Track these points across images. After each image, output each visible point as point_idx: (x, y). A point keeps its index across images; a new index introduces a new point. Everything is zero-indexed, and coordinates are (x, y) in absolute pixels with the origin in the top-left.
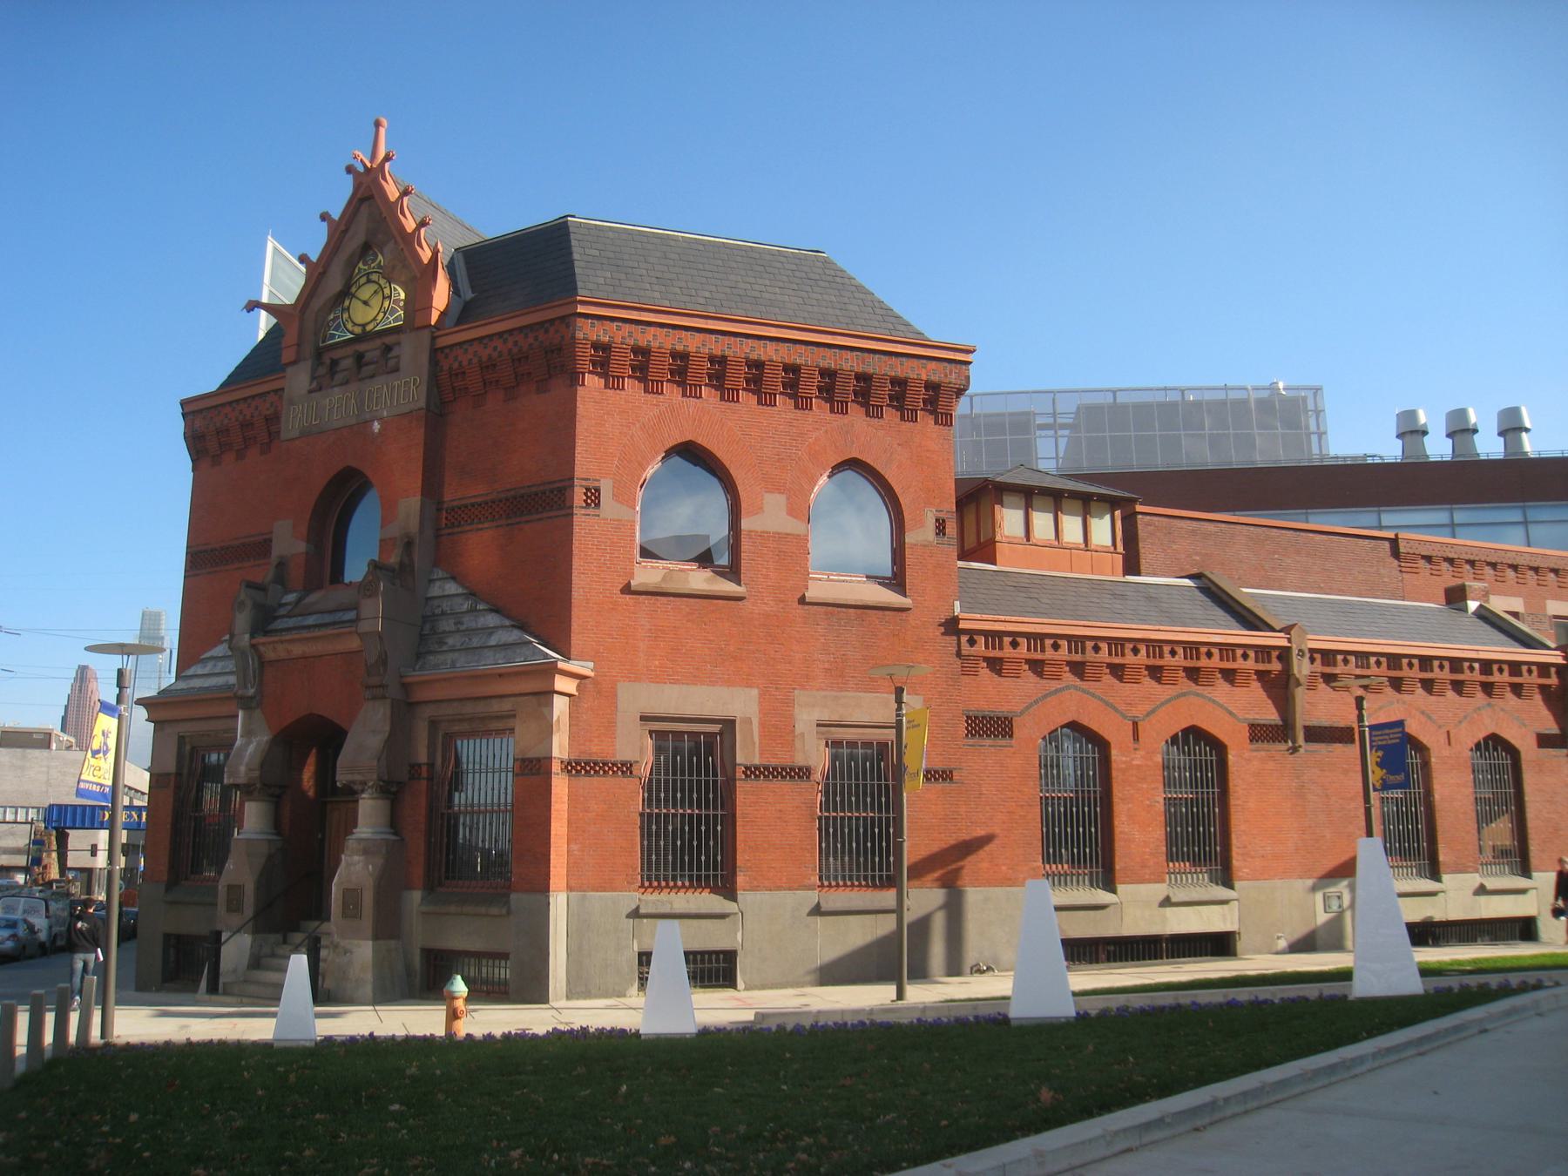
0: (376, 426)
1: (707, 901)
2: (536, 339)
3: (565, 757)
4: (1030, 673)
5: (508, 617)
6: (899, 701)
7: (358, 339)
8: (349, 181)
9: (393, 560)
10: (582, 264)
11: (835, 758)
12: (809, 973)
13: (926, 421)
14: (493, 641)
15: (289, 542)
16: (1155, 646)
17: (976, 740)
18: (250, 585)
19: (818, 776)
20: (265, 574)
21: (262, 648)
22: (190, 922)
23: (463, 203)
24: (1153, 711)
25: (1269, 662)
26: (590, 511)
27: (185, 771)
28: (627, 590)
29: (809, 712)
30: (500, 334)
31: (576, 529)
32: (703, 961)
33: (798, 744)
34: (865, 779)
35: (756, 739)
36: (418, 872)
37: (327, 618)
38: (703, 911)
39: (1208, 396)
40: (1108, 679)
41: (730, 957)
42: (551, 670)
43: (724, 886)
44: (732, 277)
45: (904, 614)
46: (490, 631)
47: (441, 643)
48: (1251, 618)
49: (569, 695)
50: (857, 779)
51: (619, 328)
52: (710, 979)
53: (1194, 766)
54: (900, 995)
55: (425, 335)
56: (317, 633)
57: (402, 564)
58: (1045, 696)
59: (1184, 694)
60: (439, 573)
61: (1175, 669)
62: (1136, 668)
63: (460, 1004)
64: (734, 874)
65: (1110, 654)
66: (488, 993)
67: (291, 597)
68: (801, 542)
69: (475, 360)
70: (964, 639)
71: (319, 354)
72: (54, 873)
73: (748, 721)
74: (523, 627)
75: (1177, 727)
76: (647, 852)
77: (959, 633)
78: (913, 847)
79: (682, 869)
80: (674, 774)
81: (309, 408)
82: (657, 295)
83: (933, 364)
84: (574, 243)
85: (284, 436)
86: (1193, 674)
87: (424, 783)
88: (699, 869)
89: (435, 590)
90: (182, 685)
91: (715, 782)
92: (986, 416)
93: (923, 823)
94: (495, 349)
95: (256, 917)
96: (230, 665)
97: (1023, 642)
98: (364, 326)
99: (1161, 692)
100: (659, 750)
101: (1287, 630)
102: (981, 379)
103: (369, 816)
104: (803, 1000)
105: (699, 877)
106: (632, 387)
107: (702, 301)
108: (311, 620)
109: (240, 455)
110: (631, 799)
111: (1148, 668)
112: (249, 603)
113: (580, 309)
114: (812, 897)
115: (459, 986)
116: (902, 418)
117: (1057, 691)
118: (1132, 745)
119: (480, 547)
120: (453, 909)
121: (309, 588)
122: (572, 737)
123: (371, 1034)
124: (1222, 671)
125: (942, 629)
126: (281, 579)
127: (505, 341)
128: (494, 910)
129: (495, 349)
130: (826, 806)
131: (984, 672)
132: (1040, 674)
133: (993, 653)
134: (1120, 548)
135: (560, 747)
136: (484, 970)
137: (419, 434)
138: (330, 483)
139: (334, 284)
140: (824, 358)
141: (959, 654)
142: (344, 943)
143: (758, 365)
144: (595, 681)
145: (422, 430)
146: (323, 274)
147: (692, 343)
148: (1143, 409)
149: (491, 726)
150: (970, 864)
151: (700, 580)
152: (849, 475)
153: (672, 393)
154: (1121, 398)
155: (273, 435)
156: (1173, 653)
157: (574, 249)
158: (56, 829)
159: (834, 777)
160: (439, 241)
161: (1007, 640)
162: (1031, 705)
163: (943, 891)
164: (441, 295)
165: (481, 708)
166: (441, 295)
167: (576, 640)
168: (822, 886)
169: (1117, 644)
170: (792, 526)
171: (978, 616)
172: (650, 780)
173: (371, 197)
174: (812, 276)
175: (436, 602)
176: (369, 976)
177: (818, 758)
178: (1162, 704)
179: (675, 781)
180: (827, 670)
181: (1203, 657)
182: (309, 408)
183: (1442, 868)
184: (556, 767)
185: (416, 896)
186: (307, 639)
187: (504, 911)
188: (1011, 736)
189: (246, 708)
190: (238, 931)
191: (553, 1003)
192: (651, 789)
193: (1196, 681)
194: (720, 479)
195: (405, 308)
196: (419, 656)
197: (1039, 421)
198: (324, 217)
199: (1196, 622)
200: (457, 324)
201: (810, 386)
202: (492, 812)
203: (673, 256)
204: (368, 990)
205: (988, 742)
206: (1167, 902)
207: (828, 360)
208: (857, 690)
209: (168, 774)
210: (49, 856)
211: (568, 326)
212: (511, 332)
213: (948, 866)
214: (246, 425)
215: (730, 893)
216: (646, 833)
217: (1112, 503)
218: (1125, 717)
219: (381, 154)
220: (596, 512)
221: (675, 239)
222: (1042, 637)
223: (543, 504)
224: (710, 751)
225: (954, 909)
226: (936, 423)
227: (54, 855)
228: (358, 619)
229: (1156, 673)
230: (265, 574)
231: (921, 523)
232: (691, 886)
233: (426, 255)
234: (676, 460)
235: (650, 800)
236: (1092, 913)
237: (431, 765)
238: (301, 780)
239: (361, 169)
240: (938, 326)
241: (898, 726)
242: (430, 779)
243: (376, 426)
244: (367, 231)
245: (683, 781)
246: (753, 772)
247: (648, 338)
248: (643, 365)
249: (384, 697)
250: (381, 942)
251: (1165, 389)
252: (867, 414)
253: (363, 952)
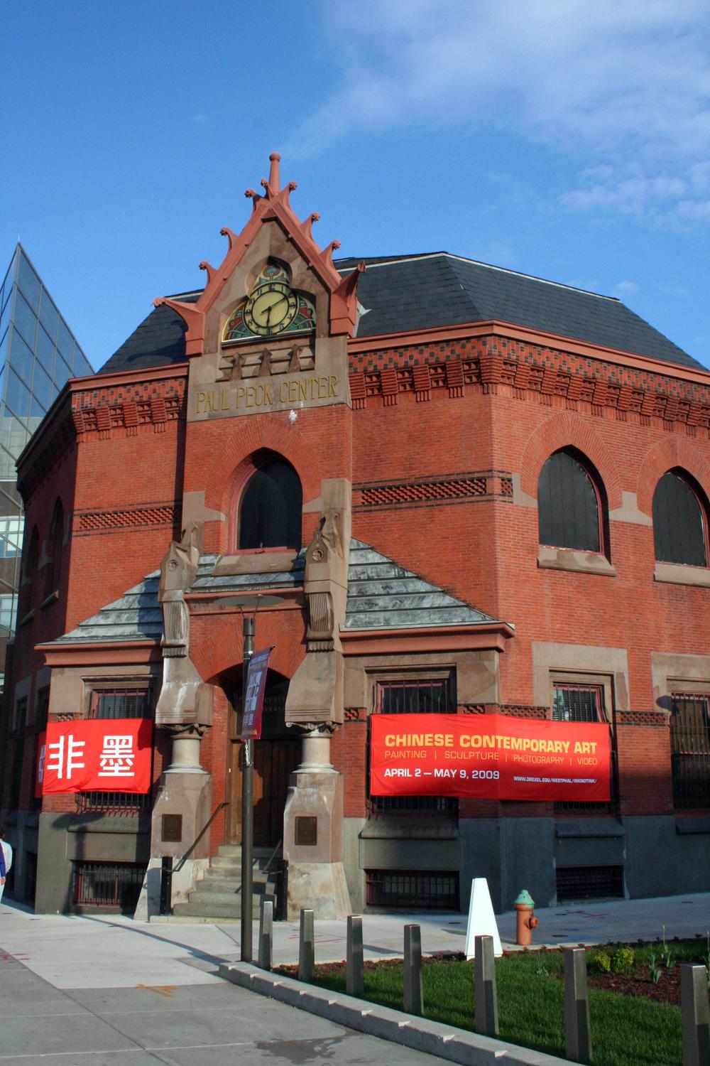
0: (293, 415)
2: (453, 352)
26: (506, 498)
35: (628, 692)
41: (617, 871)
94: (411, 357)
129: (411, 357)
180: (672, 636)
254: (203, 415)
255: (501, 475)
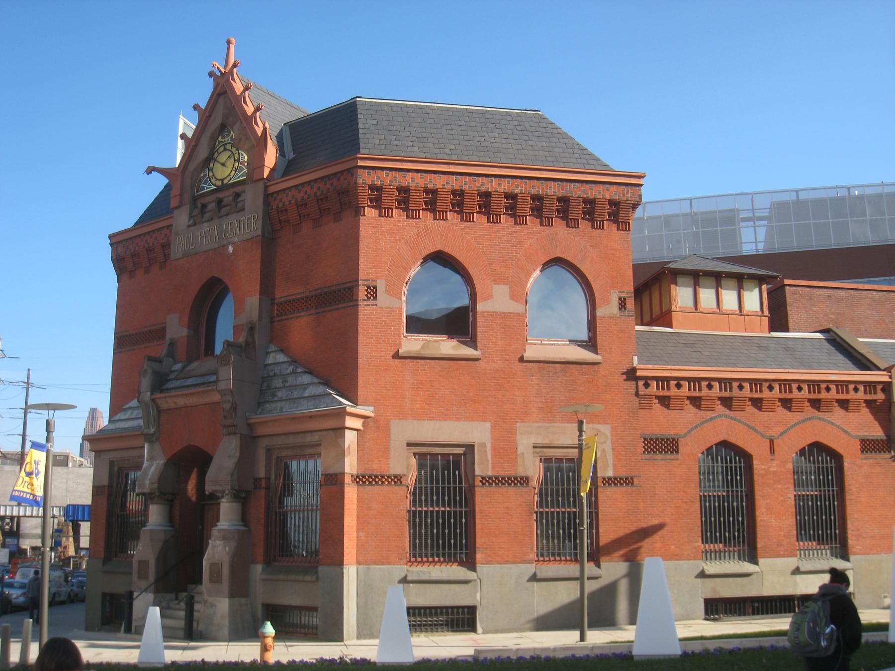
0: (231, 249)
1: (456, 571)
2: (332, 184)
3: (355, 472)
4: (691, 407)
5: (317, 376)
6: (580, 430)
7: (219, 189)
8: (211, 81)
9: (241, 340)
10: (365, 131)
11: (547, 470)
12: (528, 622)
13: (610, 228)
14: (307, 394)
15: (177, 329)
16: (786, 384)
17: (651, 455)
18: (151, 359)
19: (534, 483)
20: (160, 351)
21: (159, 401)
22: (117, 586)
23: (285, 92)
24: (785, 432)
25: (875, 393)
26: (370, 302)
27: (115, 485)
28: (397, 356)
29: (526, 439)
30: (309, 182)
31: (361, 315)
32: (452, 613)
33: (519, 460)
34: (568, 484)
36: (260, 551)
37: (200, 380)
38: (452, 578)
39: (868, 191)
40: (751, 409)
41: (471, 610)
42: (342, 413)
43: (467, 561)
44: (471, 133)
45: (596, 367)
46: (305, 386)
47: (274, 395)
48: (864, 361)
49: (357, 430)
50: (563, 484)
51: (387, 175)
52: (463, 626)
53: (818, 472)
54: (582, 638)
55: (261, 186)
56: (192, 390)
57: (247, 343)
58: (703, 423)
59: (809, 419)
60: (273, 348)
61: (802, 401)
62: (771, 401)
63: (269, 641)
64: (475, 553)
65: (751, 390)
66: (306, 634)
67: (178, 366)
68: (520, 318)
69: (293, 201)
70: (641, 383)
71: (195, 200)
72: (71, 552)
73: (483, 445)
74: (327, 384)
75: (805, 442)
76: (413, 537)
77: (637, 379)
78: (607, 533)
79: (438, 549)
80: (432, 483)
81: (189, 238)
82: (416, 149)
83: (614, 188)
84: (359, 116)
85: (172, 257)
86: (816, 404)
87: (263, 492)
88: (450, 549)
89: (270, 360)
90: (112, 427)
91: (460, 488)
92: (702, 213)
93: (615, 516)
94: (306, 193)
95: (157, 581)
96: (138, 413)
97: (685, 384)
98: (222, 180)
99: (792, 417)
100: (421, 467)
101: (888, 369)
102: (647, 194)
103: (227, 515)
104: (517, 641)
105: (449, 555)
106: (398, 215)
107: (448, 151)
108: (189, 382)
109: (147, 271)
110: (401, 501)
111: (780, 400)
112: (150, 371)
113: (360, 163)
114: (530, 569)
115: (269, 629)
116: (593, 227)
117: (711, 419)
118: (769, 457)
119: (301, 329)
120: (281, 577)
121: (189, 361)
122: (359, 459)
123: (203, 660)
124: (838, 401)
125: (625, 377)
126: (171, 354)
127: (312, 187)
128: (308, 578)
129: (306, 193)
130: (540, 504)
131: (656, 406)
132: (698, 407)
133: (664, 393)
134: (766, 312)
135: (351, 465)
136: (303, 618)
137: (258, 253)
138: (203, 286)
139: (203, 152)
140: (534, 187)
141: (637, 394)
142: (211, 600)
143: (487, 195)
144: (375, 420)
145: (259, 251)
146: (195, 146)
147: (439, 182)
148: (820, 204)
149: (309, 451)
150: (646, 544)
151: (447, 346)
152: (556, 270)
153: (426, 218)
154: (803, 196)
155: (166, 256)
156: (800, 389)
157: (360, 121)
158: (72, 521)
159: (546, 484)
160: (270, 122)
161: (673, 383)
162: (692, 430)
163: (627, 563)
164: (271, 157)
165: (299, 440)
166: (271, 157)
167: (361, 392)
168: (538, 561)
169: (756, 383)
170: (518, 308)
171: (650, 366)
172: (415, 488)
173: (225, 92)
174: (529, 129)
175: (271, 368)
176: (226, 622)
177: (534, 470)
178: (792, 427)
179: (432, 488)
180: (540, 408)
181: (823, 391)
182: (189, 238)
183: (759, 551)
184: (348, 480)
185: (259, 568)
186: (186, 395)
187: (314, 578)
188: (677, 452)
189: (151, 442)
190: (145, 590)
191: (346, 642)
192: (416, 495)
193: (818, 409)
194: (462, 276)
195: (248, 167)
196: (259, 404)
197: (742, 215)
198: (196, 107)
199: (820, 365)
200: (282, 177)
201: (525, 207)
202: (299, 511)
203: (429, 121)
204: (226, 631)
205: (660, 456)
206: (797, 571)
207: (537, 189)
208: (562, 422)
209: (104, 487)
210: (68, 540)
211: (352, 175)
212: (315, 180)
213: (631, 545)
214: (149, 250)
215: (471, 564)
216: (413, 525)
217: (760, 280)
218: (763, 436)
219: (232, 62)
220: (375, 303)
221: (432, 108)
222: (699, 380)
223: (340, 297)
224: (457, 466)
225: (634, 577)
226: (618, 229)
227: (71, 539)
228: (217, 381)
229: (787, 404)
230: (160, 351)
231: (608, 302)
232: (445, 561)
233: (259, 131)
234: (431, 264)
235: (414, 501)
236: (739, 579)
237: (268, 479)
238: (186, 490)
239: (218, 74)
240: (618, 159)
241: (580, 447)
242: (267, 488)
243: (231, 249)
244: (223, 117)
245: (438, 488)
246: (487, 481)
247: (408, 180)
248: (405, 200)
249: (235, 433)
250: (236, 599)
251: (837, 187)
252: (567, 226)
253: (223, 605)
254: (180, 255)
255: (366, 283)
